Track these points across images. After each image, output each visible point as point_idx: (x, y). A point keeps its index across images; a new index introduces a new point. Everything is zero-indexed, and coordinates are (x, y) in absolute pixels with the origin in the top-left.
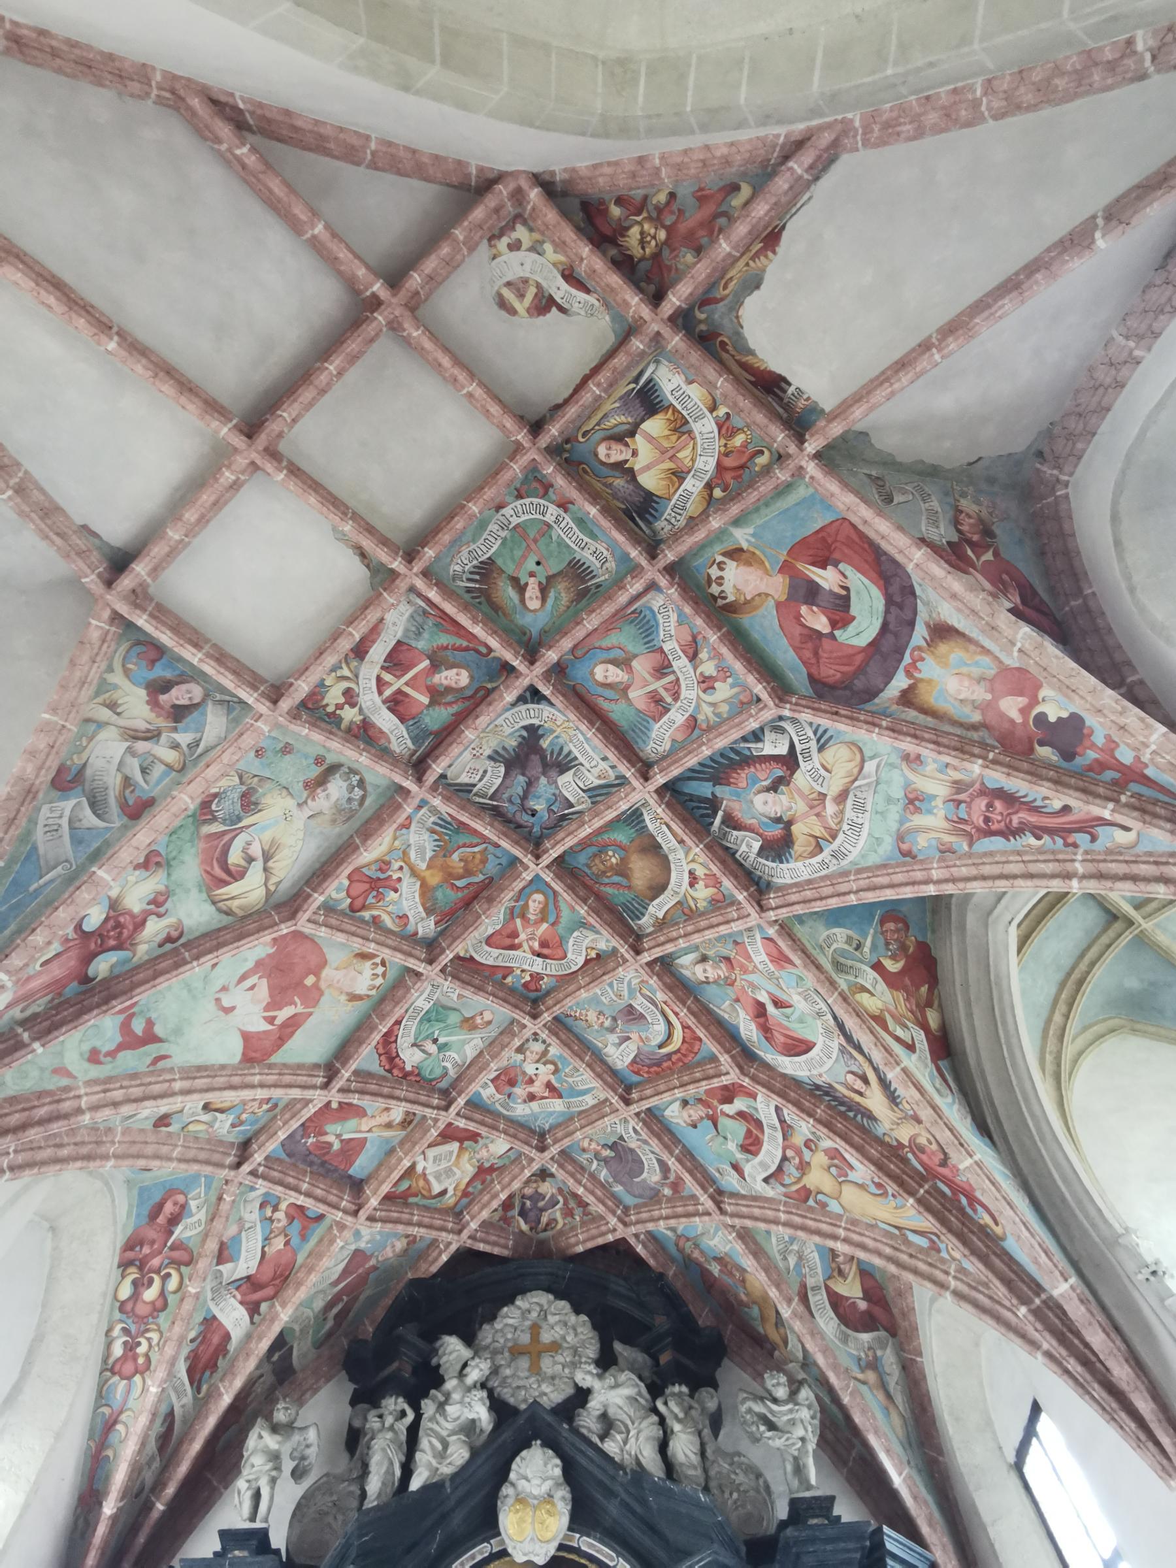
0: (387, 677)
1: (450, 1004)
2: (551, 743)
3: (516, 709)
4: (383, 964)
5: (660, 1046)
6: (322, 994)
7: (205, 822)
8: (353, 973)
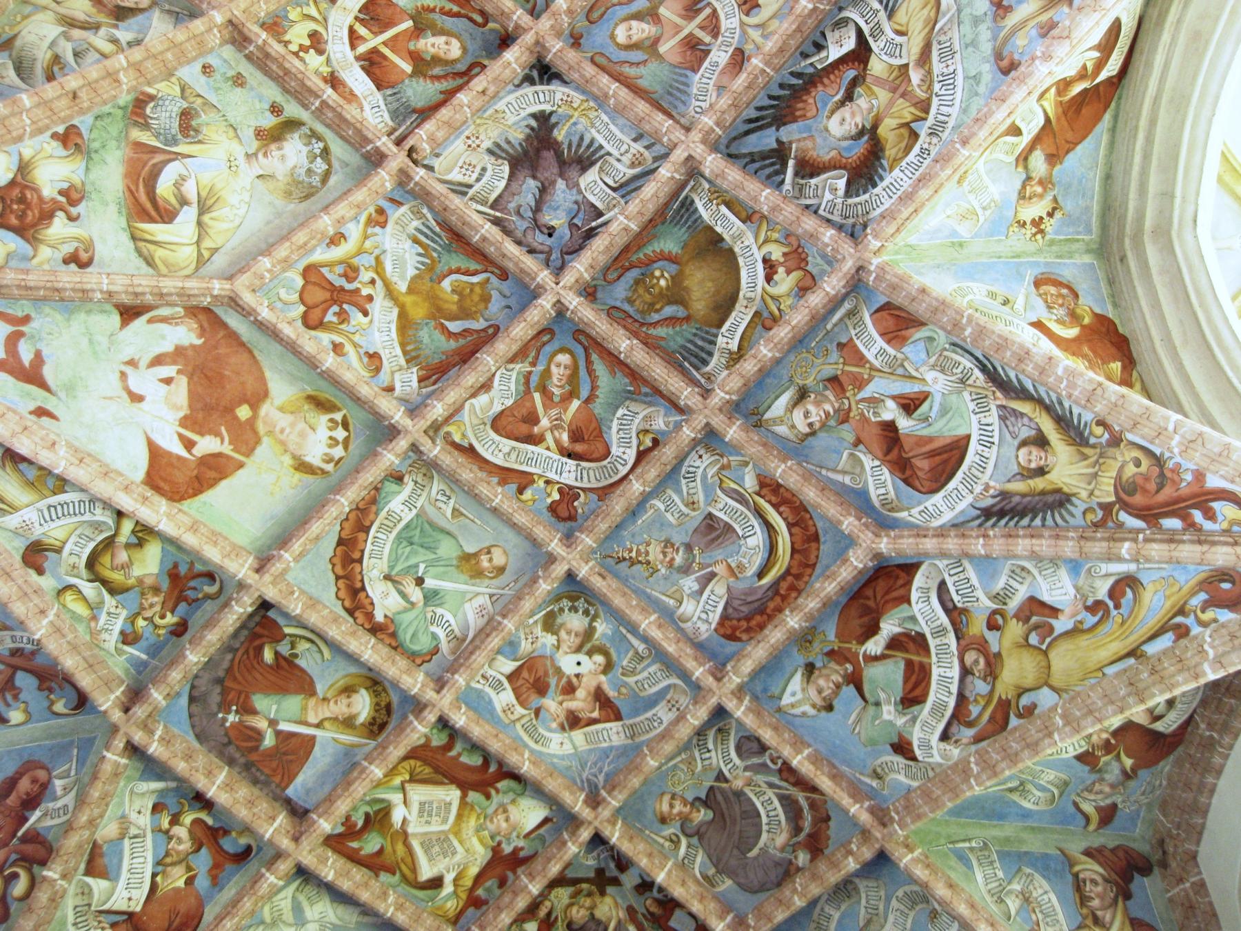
0: (362, 30)
1: (442, 523)
2: (568, 134)
4: (345, 425)
5: (760, 575)
6: (258, 441)
7: (136, 124)
8: (301, 425)
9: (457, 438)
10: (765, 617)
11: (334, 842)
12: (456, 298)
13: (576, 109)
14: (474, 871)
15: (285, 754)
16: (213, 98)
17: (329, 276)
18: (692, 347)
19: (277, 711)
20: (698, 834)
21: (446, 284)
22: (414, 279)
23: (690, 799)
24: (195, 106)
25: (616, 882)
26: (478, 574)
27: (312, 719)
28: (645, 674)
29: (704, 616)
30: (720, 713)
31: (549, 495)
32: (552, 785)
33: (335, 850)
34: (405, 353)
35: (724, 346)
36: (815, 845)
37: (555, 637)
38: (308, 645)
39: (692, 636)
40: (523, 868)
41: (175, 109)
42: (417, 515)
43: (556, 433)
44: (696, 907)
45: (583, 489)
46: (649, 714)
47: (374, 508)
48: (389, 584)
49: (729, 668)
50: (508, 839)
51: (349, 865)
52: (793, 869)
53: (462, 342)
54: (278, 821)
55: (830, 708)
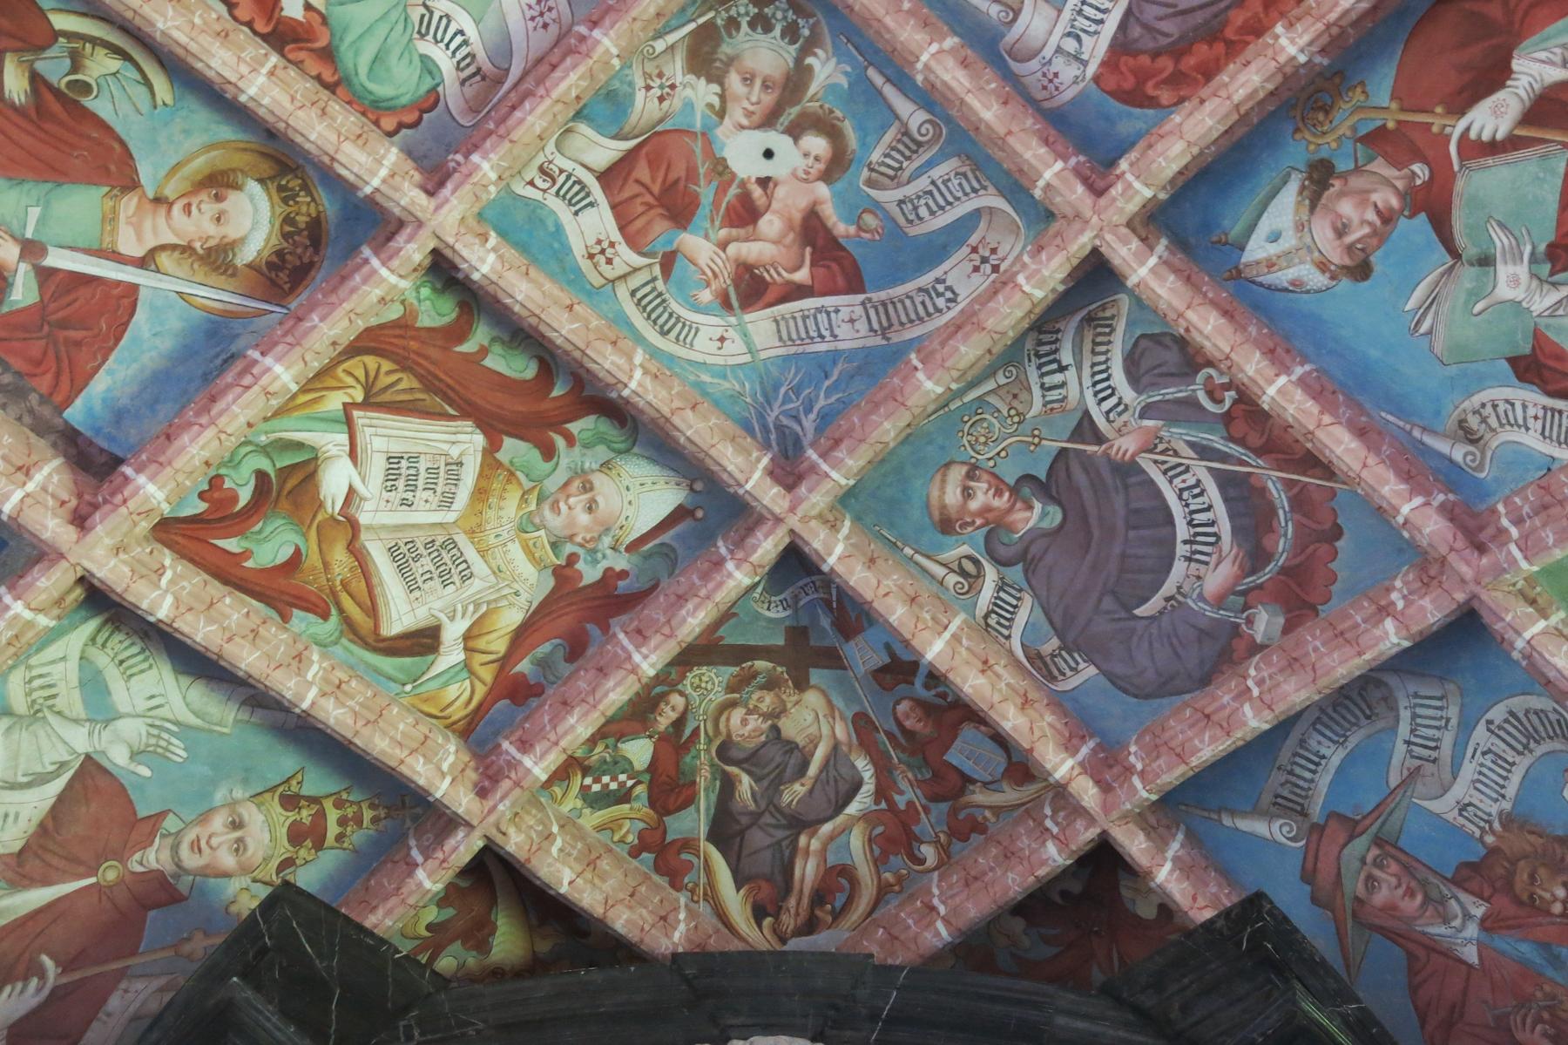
10: (1220, 48)
11: (190, 535)
14: (512, 618)
15: (64, 324)
19: (42, 221)
20: (1024, 558)
23: (1011, 481)
25: (832, 659)
27: (130, 245)
28: (923, 183)
29: (1070, 45)
30: (1095, 277)
32: (698, 429)
33: (182, 554)
36: (1300, 595)
37: (716, 88)
38: (114, 64)
39: (1040, 95)
40: (624, 618)
44: (1012, 720)
46: (926, 280)
49: (1124, 165)
50: (594, 551)
51: (215, 588)
52: (1240, 646)
54: (39, 477)
55: (1361, 270)
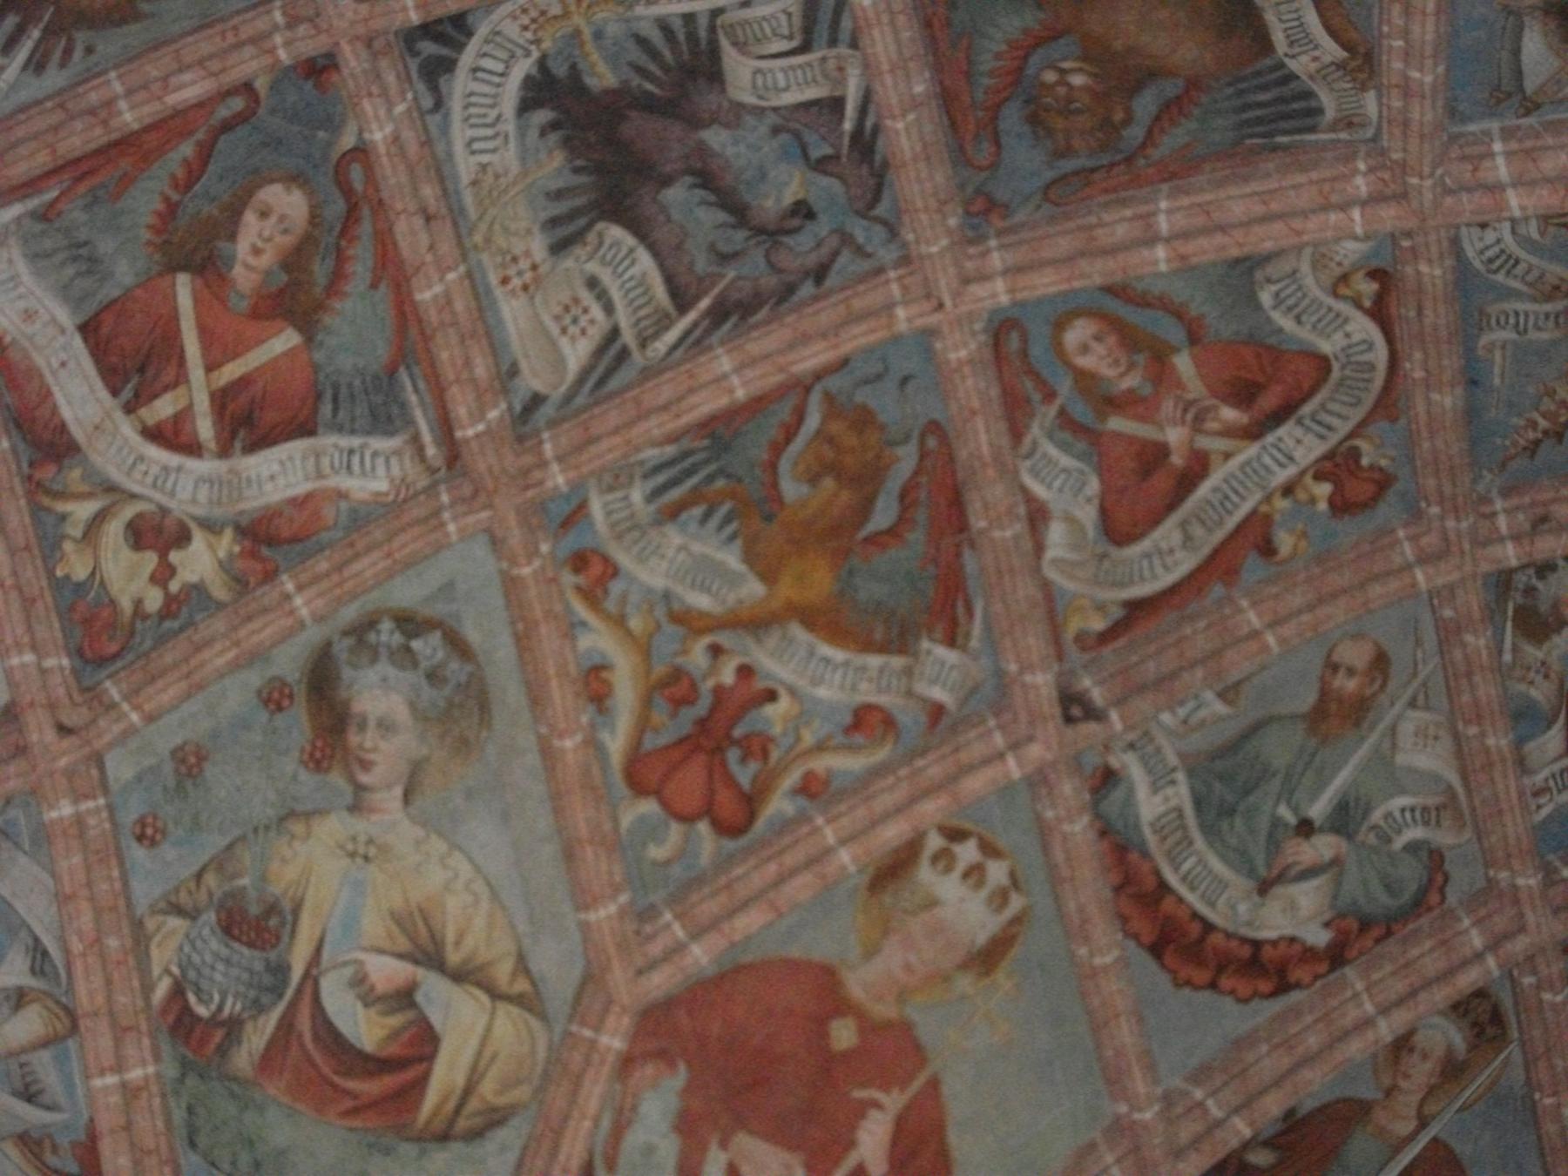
0: (163, 408)
1: (1231, 730)
2: (613, 60)
3: (456, 105)
4: (956, 835)
6: (905, 1028)
7: (223, 1051)
9: (1098, 624)
12: (828, 483)
13: (566, 14)
16: (214, 843)
17: (664, 739)
18: (1259, 113)
21: (791, 489)
22: (749, 557)
24: (218, 894)
26: (1358, 711)
27: (1404, 1128)
31: (1313, 501)
34: (883, 649)
35: (1313, 66)
41: (214, 944)
42: (1191, 773)
43: (1212, 425)
45: (1352, 435)
47: (1134, 857)
48: (1279, 890)
53: (921, 515)
